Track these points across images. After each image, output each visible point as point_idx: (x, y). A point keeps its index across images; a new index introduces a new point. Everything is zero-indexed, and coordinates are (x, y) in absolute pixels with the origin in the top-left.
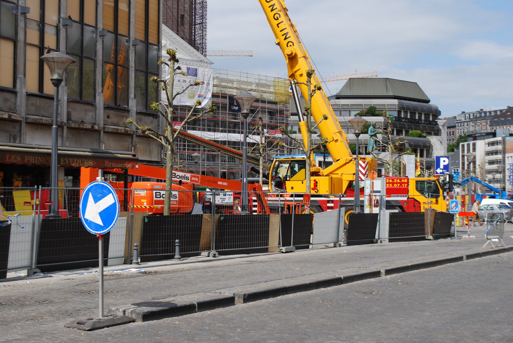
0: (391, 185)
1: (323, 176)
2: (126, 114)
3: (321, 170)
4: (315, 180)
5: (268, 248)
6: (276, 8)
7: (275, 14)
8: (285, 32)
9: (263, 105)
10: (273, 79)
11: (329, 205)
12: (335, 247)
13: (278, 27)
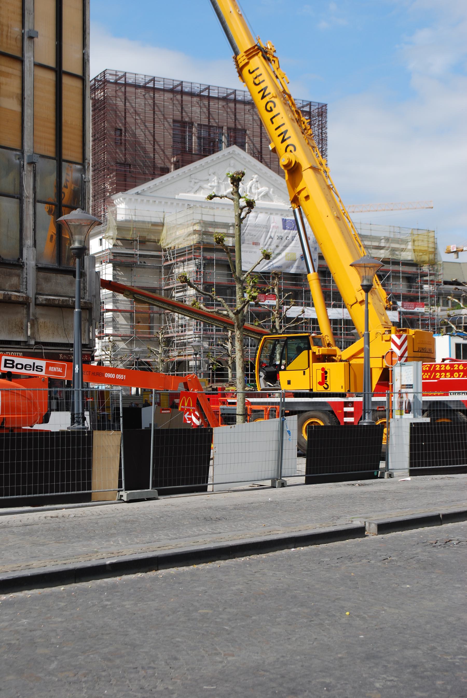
0: (448, 374)
1: (341, 361)
2: (18, 271)
3: (338, 352)
4: (323, 369)
5: (90, 494)
6: (269, 93)
7: (268, 103)
8: (282, 129)
9: (396, 268)
10: (410, 231)
11: (346, 409)
12: (273, 487)
13: (273, 123)
